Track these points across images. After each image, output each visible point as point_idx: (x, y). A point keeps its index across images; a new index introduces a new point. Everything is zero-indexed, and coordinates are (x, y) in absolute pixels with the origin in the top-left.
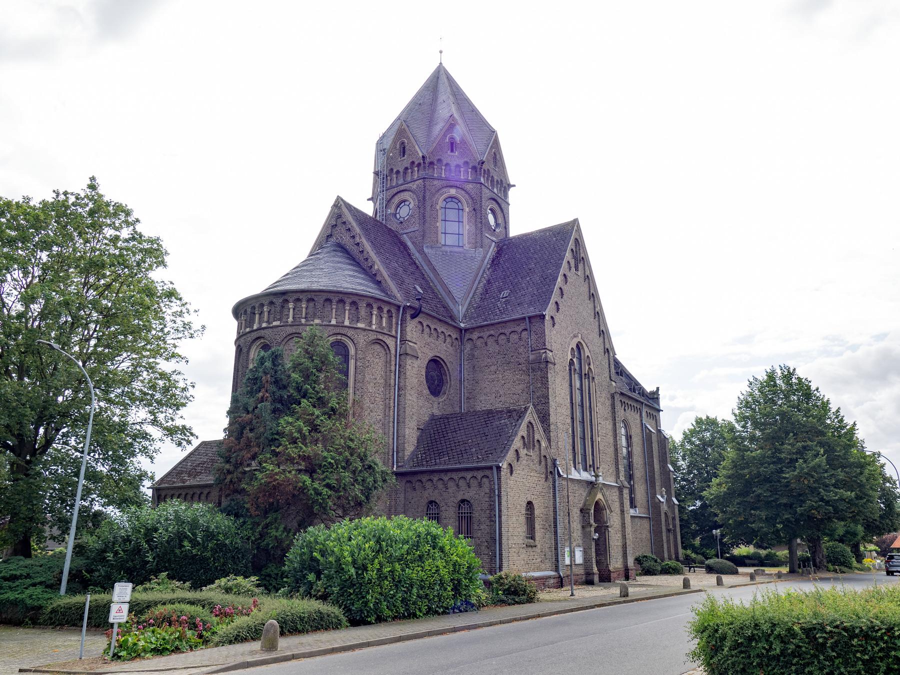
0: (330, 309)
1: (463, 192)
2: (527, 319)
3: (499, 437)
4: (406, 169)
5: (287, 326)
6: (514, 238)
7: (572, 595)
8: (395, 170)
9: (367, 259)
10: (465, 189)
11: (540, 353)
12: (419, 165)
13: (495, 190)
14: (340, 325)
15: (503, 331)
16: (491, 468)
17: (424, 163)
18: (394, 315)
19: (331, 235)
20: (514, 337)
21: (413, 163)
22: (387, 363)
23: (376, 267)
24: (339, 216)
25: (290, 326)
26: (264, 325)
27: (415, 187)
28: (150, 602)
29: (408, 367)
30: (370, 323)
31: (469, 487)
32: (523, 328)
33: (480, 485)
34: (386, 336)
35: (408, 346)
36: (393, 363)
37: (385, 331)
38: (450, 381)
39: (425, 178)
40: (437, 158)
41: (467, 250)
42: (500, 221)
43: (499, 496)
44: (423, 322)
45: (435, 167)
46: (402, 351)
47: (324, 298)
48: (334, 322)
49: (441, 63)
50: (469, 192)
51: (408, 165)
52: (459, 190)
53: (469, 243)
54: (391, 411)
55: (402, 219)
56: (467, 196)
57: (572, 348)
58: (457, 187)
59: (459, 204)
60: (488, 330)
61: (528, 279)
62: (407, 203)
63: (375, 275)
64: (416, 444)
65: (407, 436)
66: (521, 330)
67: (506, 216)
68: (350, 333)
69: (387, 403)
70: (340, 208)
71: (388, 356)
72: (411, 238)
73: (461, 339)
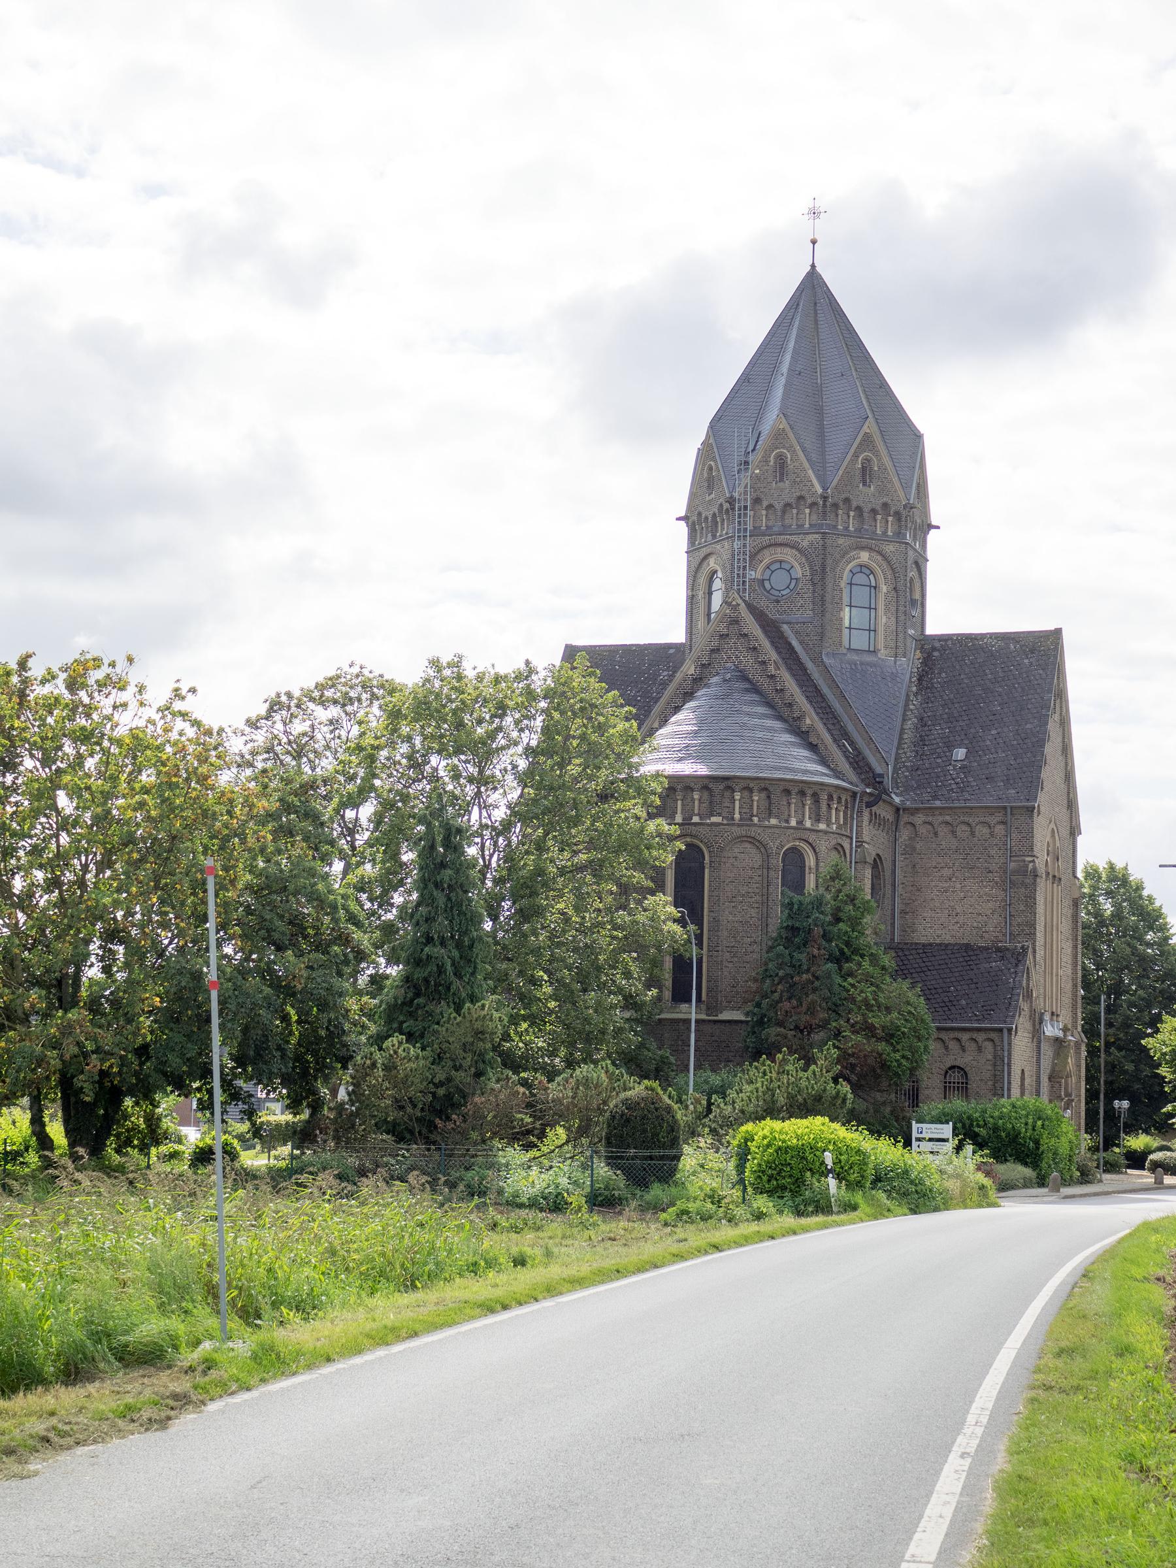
1: (879, 558)
3: (995, 988)
5: (733, 825)
8: (765, 504)
15: (966, 819)
16: (1001, 1030)
19: (718, 650)
21: (801, 498)
23: (808, 721)
25: (739, 825)
26: (696, 819)
27: (805, 544)
28: (277, 1190)
31: (964, 1051)
32: (999, 819)
33: (980, 1049)
40: (843, 496)
41: (883, 660)
43: (1009, 1065)
45: (840, 512)
46: (858, 857)
47: (782, 788)
48: (793, 823)
49: (813, 266)
51: (793, 501)
53: (886, 647)
58: (871, 549)
59: (871, 577)
60: (941, 814)
61: (994, 732)
68: (812, 838)
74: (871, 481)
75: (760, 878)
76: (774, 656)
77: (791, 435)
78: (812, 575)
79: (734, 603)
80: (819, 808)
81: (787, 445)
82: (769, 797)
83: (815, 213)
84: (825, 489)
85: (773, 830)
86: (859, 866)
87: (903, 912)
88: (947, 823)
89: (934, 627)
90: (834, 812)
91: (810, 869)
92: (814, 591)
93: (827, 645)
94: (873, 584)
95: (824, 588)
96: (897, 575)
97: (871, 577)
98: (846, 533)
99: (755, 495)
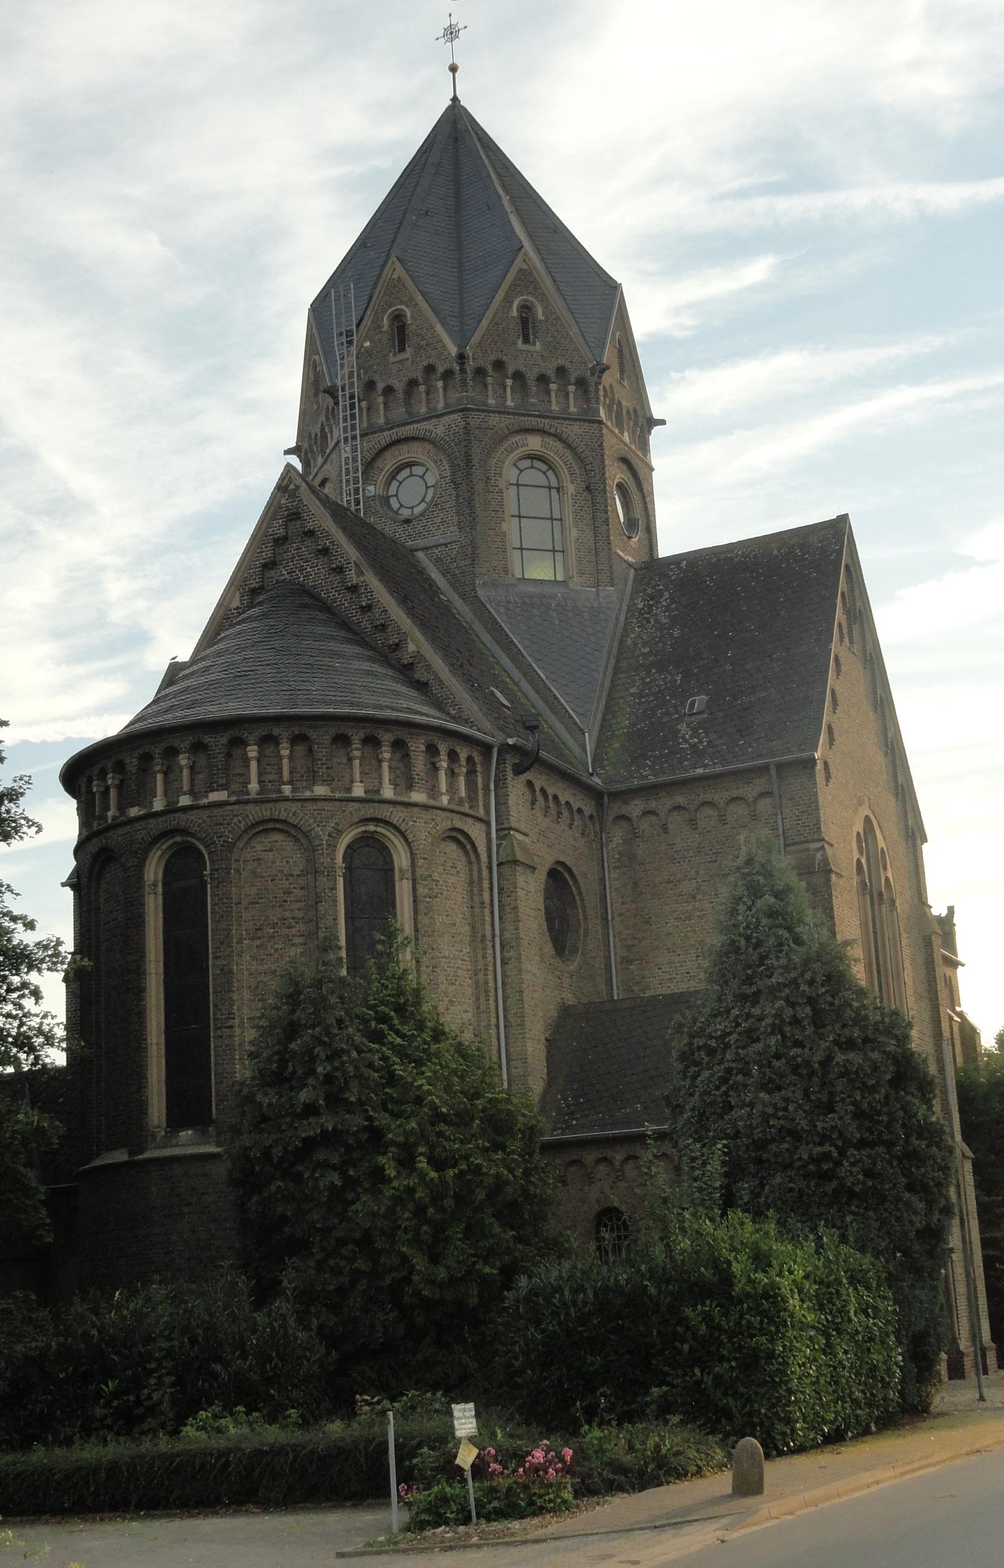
0: (344, 760)
1: (559, 445)
2: (773, 771)
4: (412, 383)
5: (248, 802)
6: (675, 560)
7: (982, 1398)
8: (380, 386)
9: (383, 627)
10: (564, 436)
11: (808, 850)
12: (448, 374)
13: (626, 437)
14: (372, 798)
17: (463, 371)
18: (479, 768)
20: (738, 811)
21: (430, 369)
22: (473, 884)
23: (411, 647)
24: (294, 516)
25: (256, 802)
26: (185, 801)
29: (521, 893)
30: (433, 792)
34: (470, 820)
35: (515, 842)
36: (486, 884)
37: (466, 808)
38: (586, 919)
39: (469, 409)
40: (493, 358)
42: (638, 513)
44: (534, 781)
45: (490, 380)
46: (502, 853)
48: (358, 791)
49: (455, 99)
50: (575, 445)
52: (551, 441)
53: (581, 574)
54: (492, 999)
55: (406, 513)
56: (569, 456)
57: (858, 834)
62: (418, 470)
63: (410, 666)
64: (545, 1077)
65: (530, 1060)
66: (755, 794)
67: (648, 499)
68: (397, 816)
69: (482, 982)
70: (294, 494)
71: (475, 868)
72: (438, 561)
73: (598, 818)
74: (535, 337)
75: (304, 893)
76: (353, 553)
77: (409, 283)
78: (453, 473)
79: (292, 487)
80: (409, 767)
81: (405, 299)
82: (310, 750)
83: (451, 33)
84: (461, 346)
85: (321, 805)
86: (506, 870)
87: (626, 961)
88: (679, 808)
89: (668, 546)
90: (442, 775)
91: (401, 871)
92: (458, 496)
93: (484, 570)
94: (554, 483)
95: (471, 490)
96: (589, 467)
97: (550, 473)
98: (502, 411)
99: (365, 378)
